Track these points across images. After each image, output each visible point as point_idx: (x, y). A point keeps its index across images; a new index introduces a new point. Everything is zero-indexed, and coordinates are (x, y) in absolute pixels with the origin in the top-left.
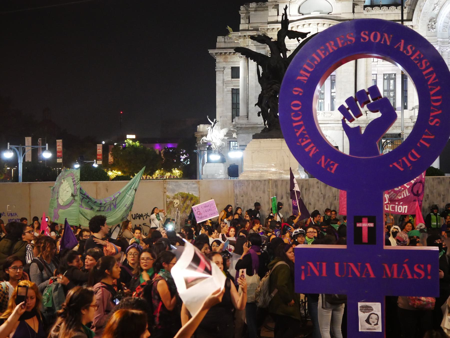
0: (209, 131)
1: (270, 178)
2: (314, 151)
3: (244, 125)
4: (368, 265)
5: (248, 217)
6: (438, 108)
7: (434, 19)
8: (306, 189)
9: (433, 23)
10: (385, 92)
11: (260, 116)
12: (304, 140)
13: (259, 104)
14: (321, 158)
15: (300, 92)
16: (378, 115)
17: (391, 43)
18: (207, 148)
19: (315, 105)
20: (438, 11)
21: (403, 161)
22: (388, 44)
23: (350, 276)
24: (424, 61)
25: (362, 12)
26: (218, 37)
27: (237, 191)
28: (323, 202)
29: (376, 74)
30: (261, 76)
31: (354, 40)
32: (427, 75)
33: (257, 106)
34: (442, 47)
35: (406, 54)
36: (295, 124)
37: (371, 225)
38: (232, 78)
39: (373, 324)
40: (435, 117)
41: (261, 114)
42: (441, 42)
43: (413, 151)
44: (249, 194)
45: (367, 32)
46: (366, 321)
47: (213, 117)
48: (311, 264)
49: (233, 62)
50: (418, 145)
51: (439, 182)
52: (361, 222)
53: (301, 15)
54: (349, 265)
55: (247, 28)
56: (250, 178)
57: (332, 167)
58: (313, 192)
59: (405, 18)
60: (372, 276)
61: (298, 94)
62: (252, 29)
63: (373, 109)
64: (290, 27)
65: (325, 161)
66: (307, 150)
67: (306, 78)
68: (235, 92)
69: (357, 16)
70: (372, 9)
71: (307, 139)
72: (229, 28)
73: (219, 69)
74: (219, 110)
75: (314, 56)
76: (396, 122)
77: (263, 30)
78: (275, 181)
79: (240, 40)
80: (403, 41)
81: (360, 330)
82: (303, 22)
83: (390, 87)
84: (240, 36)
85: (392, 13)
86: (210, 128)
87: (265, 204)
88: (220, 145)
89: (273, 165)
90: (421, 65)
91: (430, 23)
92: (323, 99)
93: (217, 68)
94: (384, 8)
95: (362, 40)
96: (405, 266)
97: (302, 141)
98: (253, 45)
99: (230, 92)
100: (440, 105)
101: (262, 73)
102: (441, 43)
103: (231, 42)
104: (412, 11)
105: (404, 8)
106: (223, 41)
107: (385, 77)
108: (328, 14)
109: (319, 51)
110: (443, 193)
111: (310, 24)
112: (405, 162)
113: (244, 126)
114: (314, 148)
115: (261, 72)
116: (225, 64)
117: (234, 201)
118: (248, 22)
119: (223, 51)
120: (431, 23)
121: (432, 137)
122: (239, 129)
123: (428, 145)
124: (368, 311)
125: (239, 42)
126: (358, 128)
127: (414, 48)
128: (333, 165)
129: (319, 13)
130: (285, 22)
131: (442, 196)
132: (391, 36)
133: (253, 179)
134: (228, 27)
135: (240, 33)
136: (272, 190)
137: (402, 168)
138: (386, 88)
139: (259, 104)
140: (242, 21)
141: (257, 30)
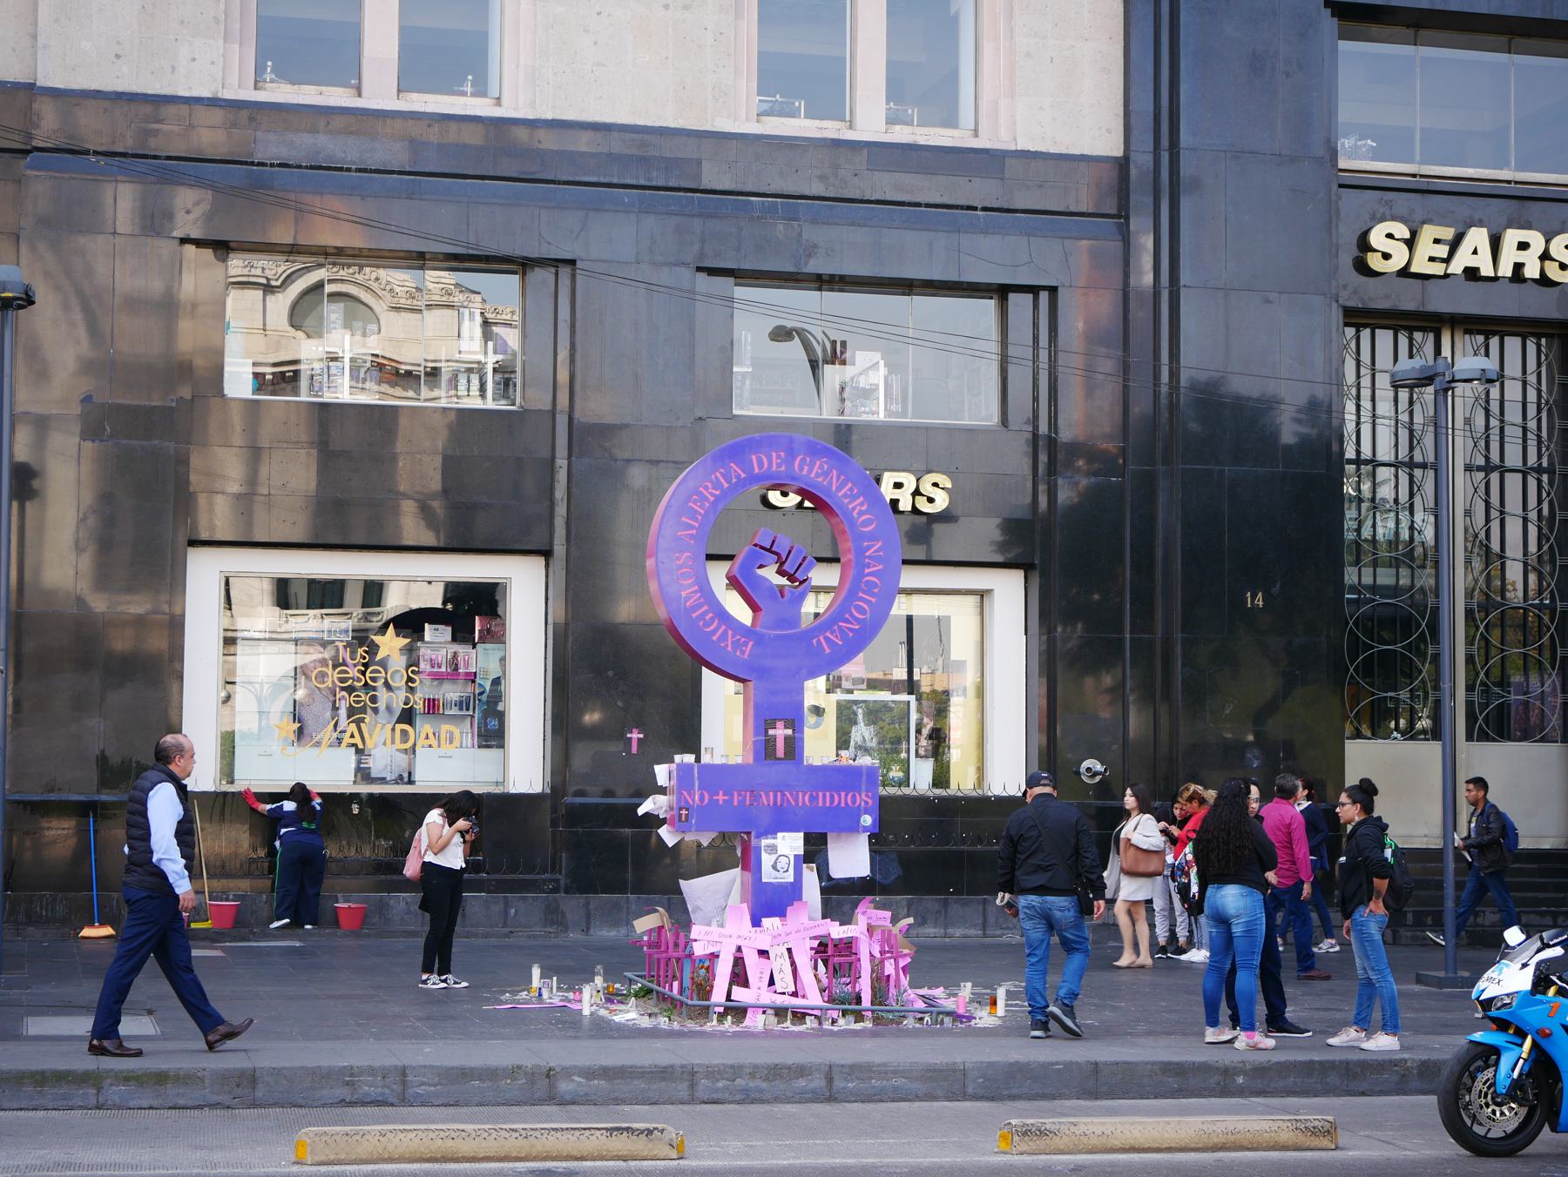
37: (789, 732)
39: (782, 871)
50: (814, 641)
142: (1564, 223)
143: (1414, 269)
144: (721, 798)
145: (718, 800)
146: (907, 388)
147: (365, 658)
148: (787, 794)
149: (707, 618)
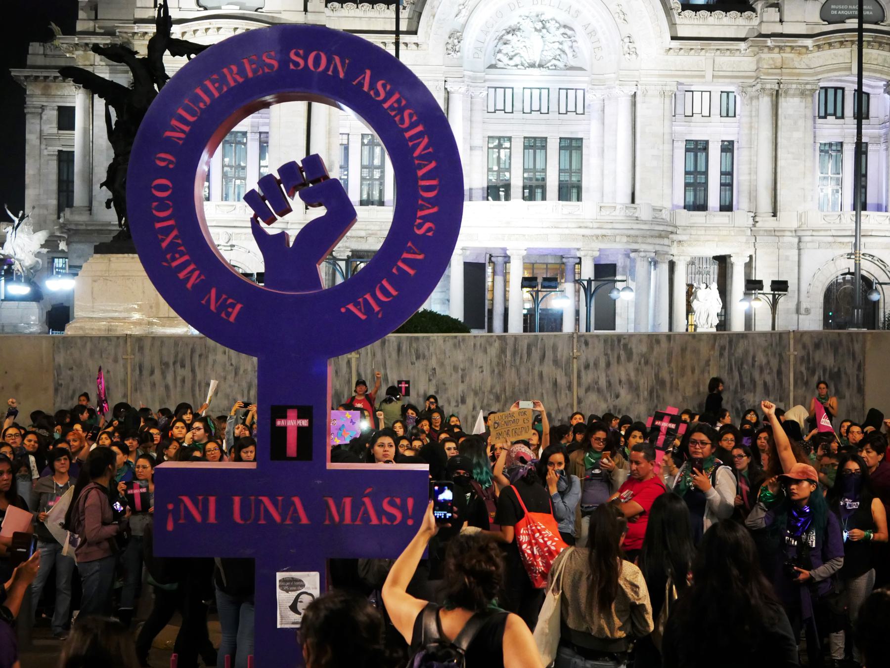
0: (9, 235)
1: (129, 332)
2: (196, 279)
3: (82, 225)
4: (296, 500)
5: (199, 429)
6: (432, 202)
7: (458, 34)
8: (200, 356)
9: (456, 41)
10: (365, 170)
11: (110, 208)
12: (177, 256)
13: (107, 184)
14: (210, 292)
15: (170, 162)
16: (320, 212)
17: (346, 74)
18: (5, 271)
19: (200, 190)
20: (466, 18)
21: (366, 300)
22: (342, 75)
23: (262, 522)
24: (406, 113)
25: (322, 10)
26: (31, 44)
27: (60, 359)
28: (235, 382)
29: (348, 134)
30: (114, 127)
31: (275, 64)
32: (412, 138)
33: (104, 188)
34: (471, 88)
35: (373, 96)
36: (158, 225)
37: (304, 423)
38: (60, 128)
40: (426, 219)
41: (112, 204)
42: (470, 77)
43: (385, 283)
44: (84, 363)
45: (301, 52)
46: (290, 607)
47: (18, 205)
48: (186, 500)
49: (62, 96)
50: (394, 271)
51: (455, 345)
52: (285, 417)
53: (202, 9)
54: (261, 500)
55: (91, 29)
56: (87, 331)
57: (230, 310)
58: (215, 361)
59: (403, 27)
60: (304, 520)
61: (167, 166)
62: (102, 31)
63: (310, 201)
64: (176, 32)
65: (218, 298)
66: (181, 275)
67: (182, 136)
68: (65, 159)
69: (312, 19)
70: (342, 7)
71: (182, 254)
72: (53, 26)
73: (33, 110)
74: (30, 194)
75: (199, 91)
76: (355, 226)
77: (124, 35)
78: (139, 340)
79: (77, 53)
80: (368, 72)
81: (279, 626)
82: (206, 23)
83: (373, 159)
84: (77, 44)
85: (379, 16)
86: (10, 229)
87: (117, 386)
88: (30, 265)
89: (136, 307)
90: (402, 120)
91: (450, 41)
92: (245, 179)
93: (29, 107)
94: (365, 7)
95: (292, 66)
96: (367, 500)
97: (174, 259)
98: (103, 63)
99: (55, 158)
100: (435, 196)
101: (117, 122)
102: (470, 80)
103: (60, 56)
104: (416, 14)
105: (401, 7)
106: (41, 52)
107: (366, 141)
108: (256, 10)
109: (208, 83)
110: (461, 366)
111: (219, 29)
112: (369, 303)
113: (83, 227)
114: (197, 273)
115: (114, 118)
116: (45, 99)
117: (54, 378)
118: (93, 17)
119: (35, 73)
120: (453, 41)
121: (420, 257)
122: (73, 233)
123: (412, 272)
124: (295, 588)
125: (74, 56)
126: (283, 236)
127: (388, 87)
128: (233, 306)
129: (238, 7)
130: (164, 22)
131: (460, 371)
132: (347, 61)
133: (94, 333)
134: (53, 25)
135: (76, 39)
136: (133, 357)
137: (364, 314)
138: (366, 163)
139: (107, 184)
140: (82, 14)
141: (111, 33)
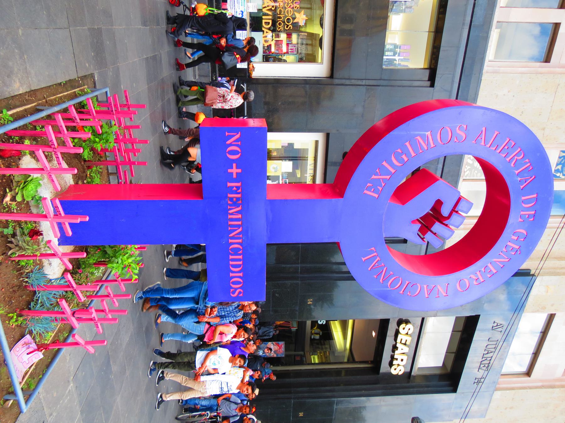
142: (406, 367)
143: (399, 335)
144: (235, 171)
145: (237, 168)
146: (420, 221)
147: (295, 7)
148: (240, 230)
149: (404, 156)
